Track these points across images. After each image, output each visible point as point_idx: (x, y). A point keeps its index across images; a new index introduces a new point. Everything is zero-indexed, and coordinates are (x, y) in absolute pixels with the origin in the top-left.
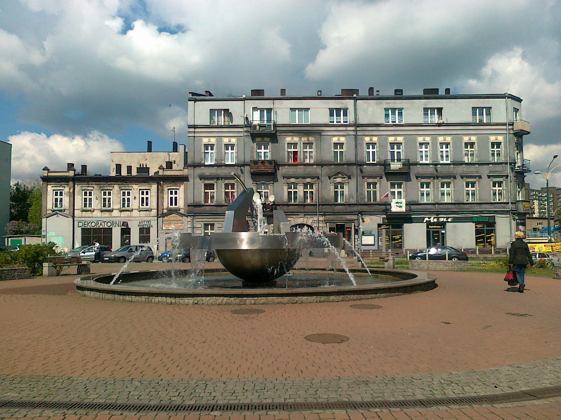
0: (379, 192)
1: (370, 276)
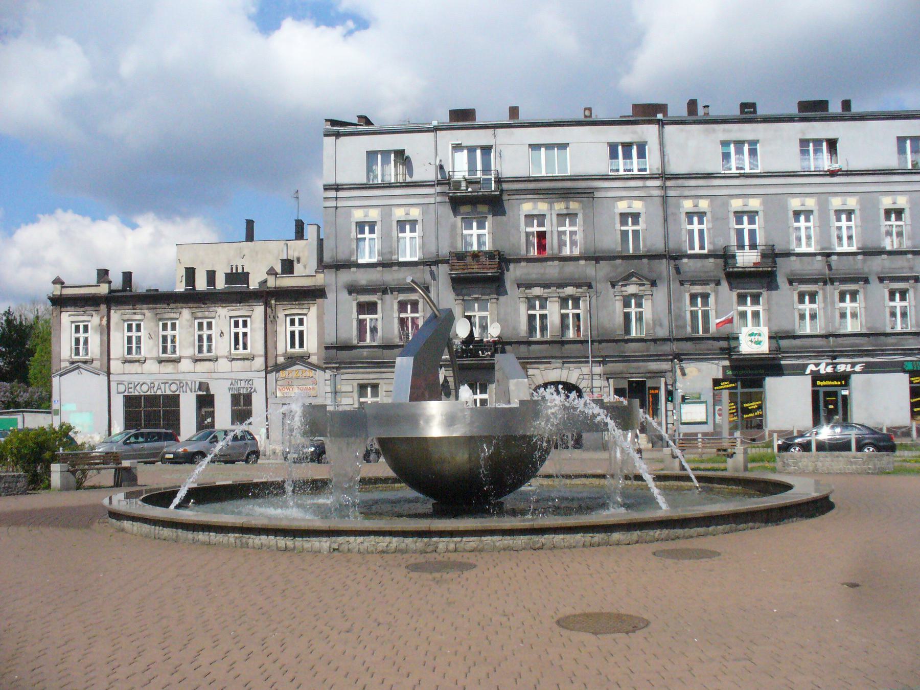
0: (714, 312)
1: (697, 488)
